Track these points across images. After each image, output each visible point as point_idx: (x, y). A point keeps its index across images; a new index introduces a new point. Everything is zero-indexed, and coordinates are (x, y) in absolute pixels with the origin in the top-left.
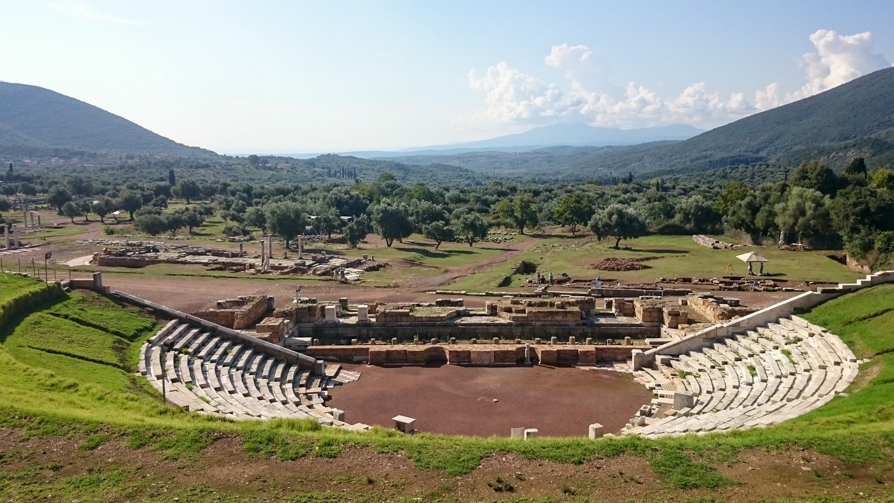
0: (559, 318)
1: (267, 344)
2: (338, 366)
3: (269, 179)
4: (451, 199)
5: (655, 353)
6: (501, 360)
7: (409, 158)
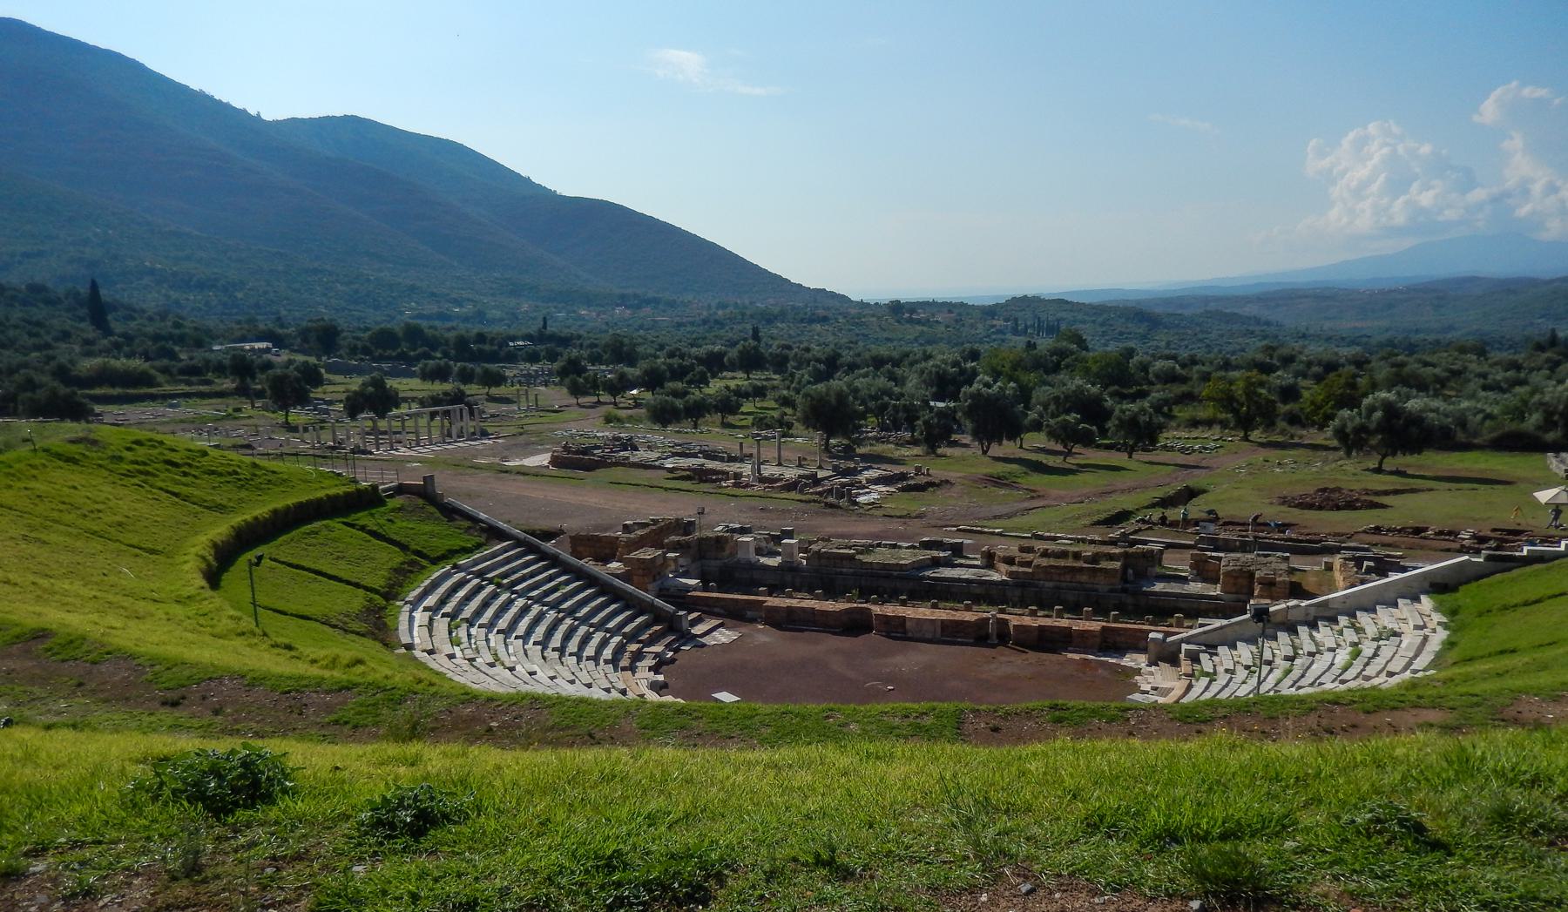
0: (1084, 578)
1: (617, 582)
3: (916, 339)
4: (1157, 376)
5: (1182, 641)
6: (951, 633)
7: (1168, 301)
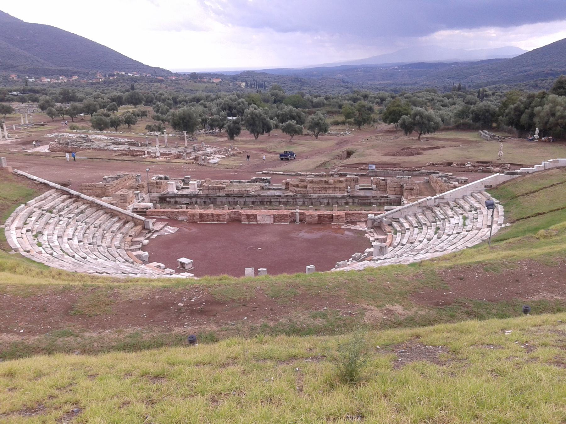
2: (166, 223)
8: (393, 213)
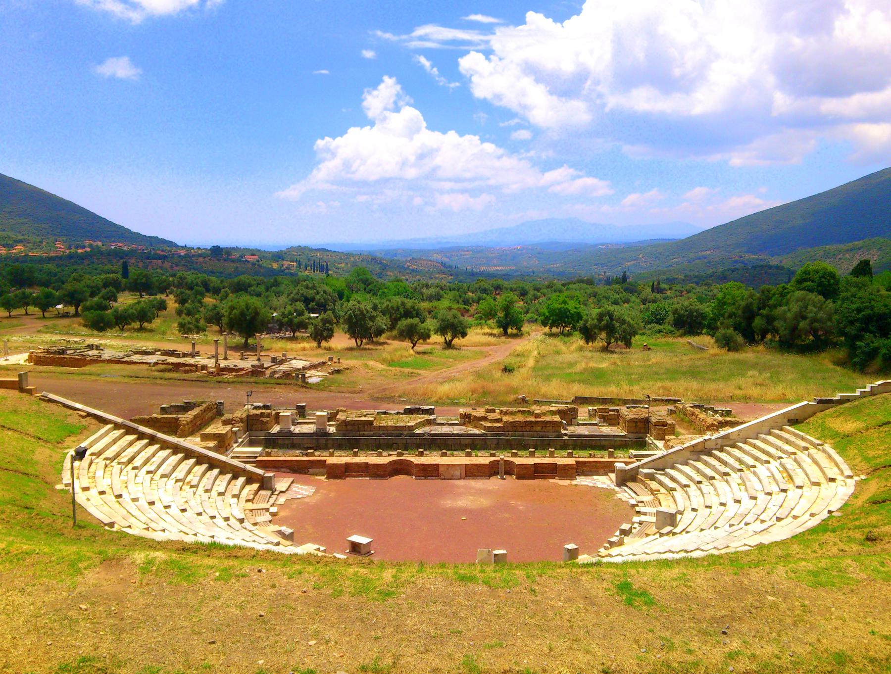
8: (653, 461)
